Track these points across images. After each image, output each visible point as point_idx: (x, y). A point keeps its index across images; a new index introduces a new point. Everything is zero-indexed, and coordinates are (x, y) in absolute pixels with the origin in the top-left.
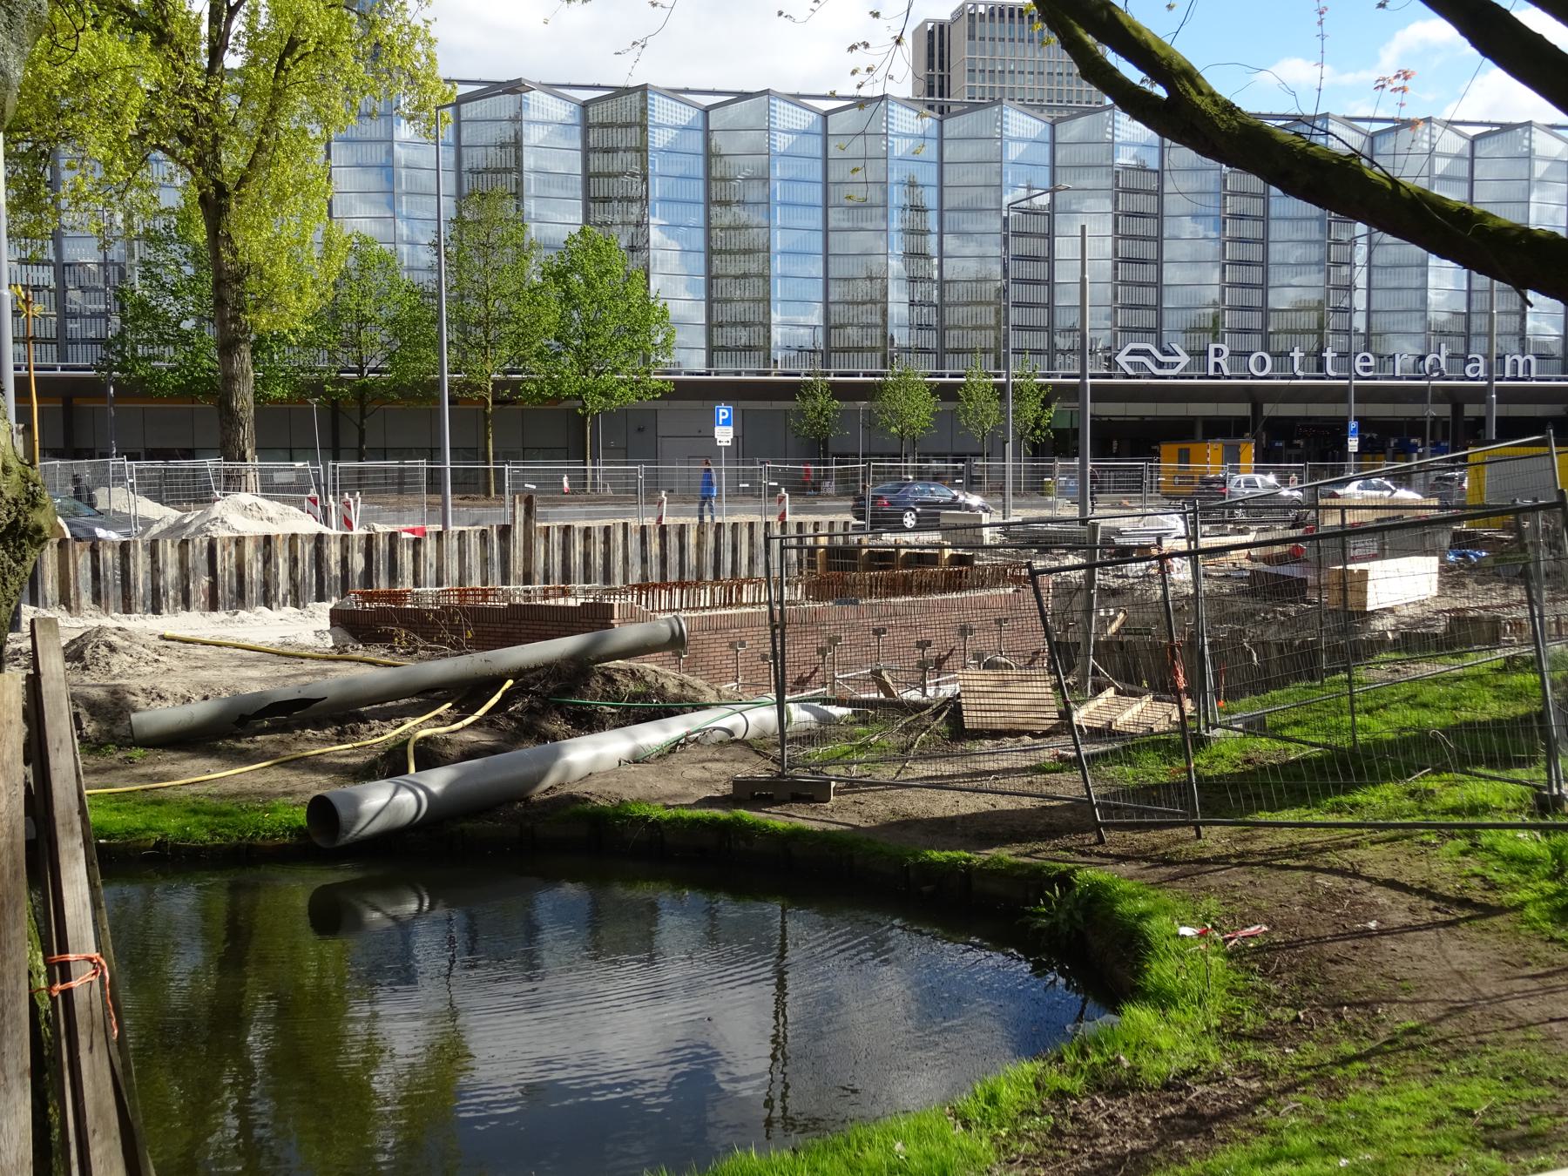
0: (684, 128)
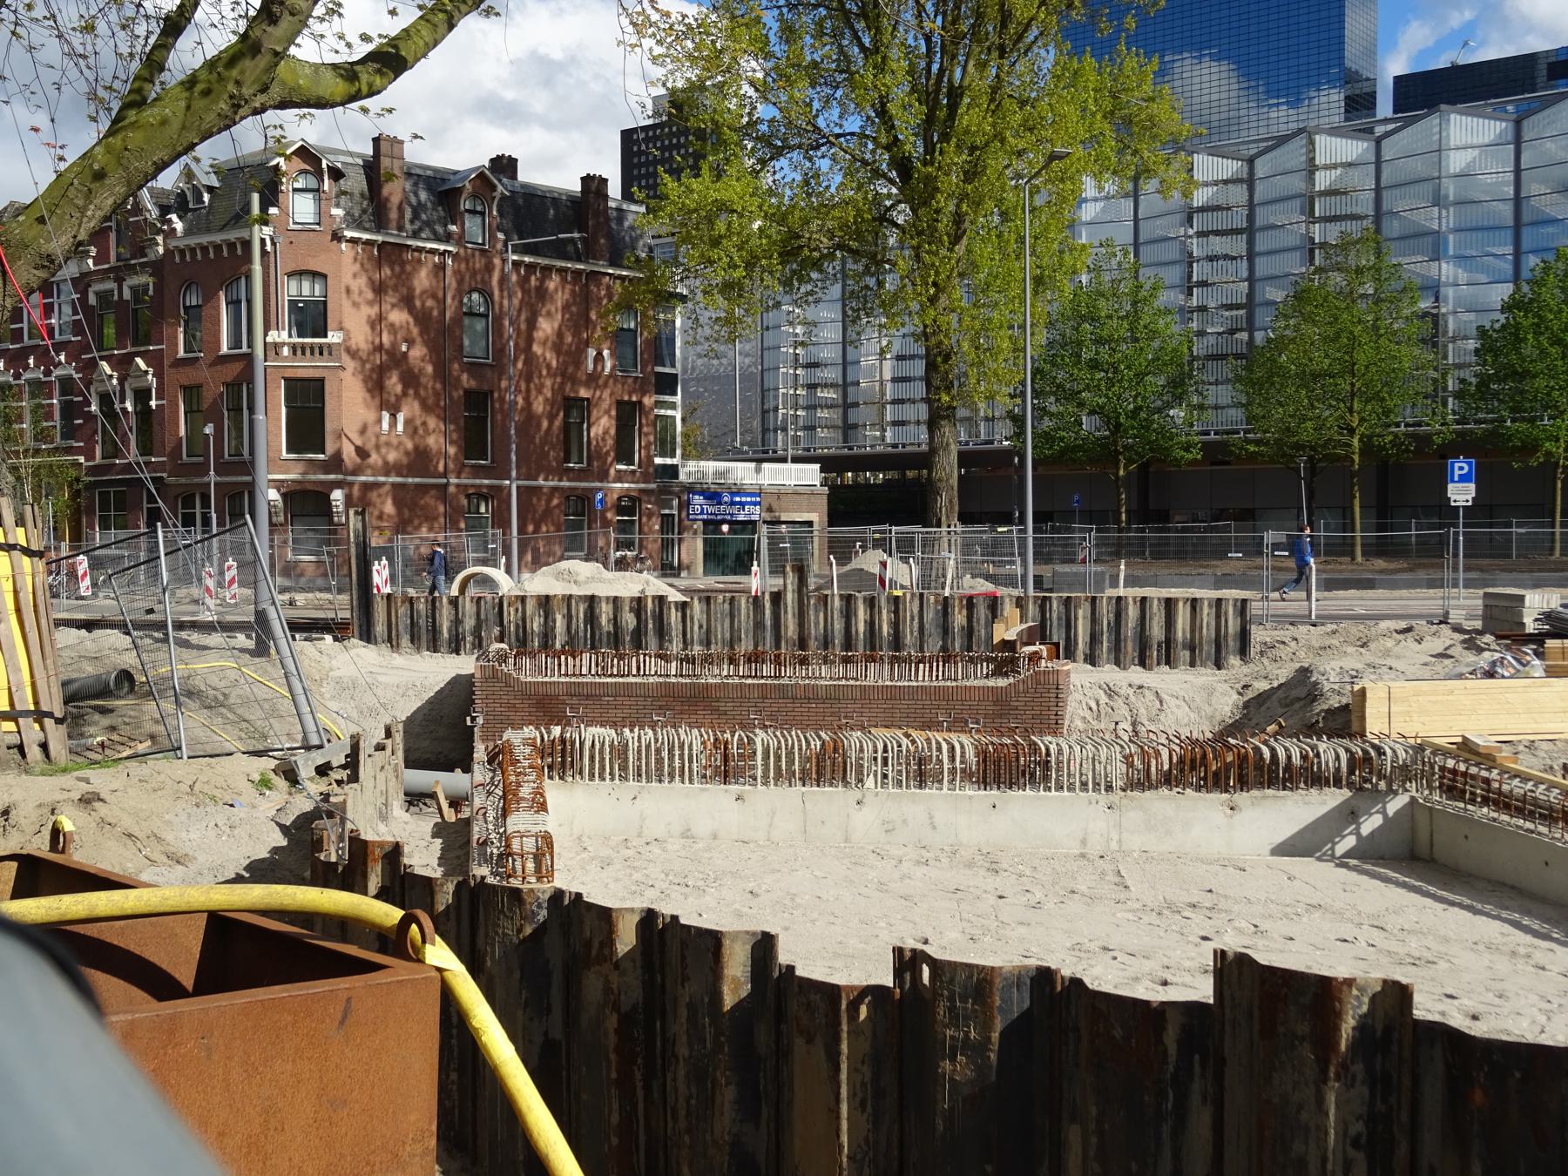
0: (1226, 182)
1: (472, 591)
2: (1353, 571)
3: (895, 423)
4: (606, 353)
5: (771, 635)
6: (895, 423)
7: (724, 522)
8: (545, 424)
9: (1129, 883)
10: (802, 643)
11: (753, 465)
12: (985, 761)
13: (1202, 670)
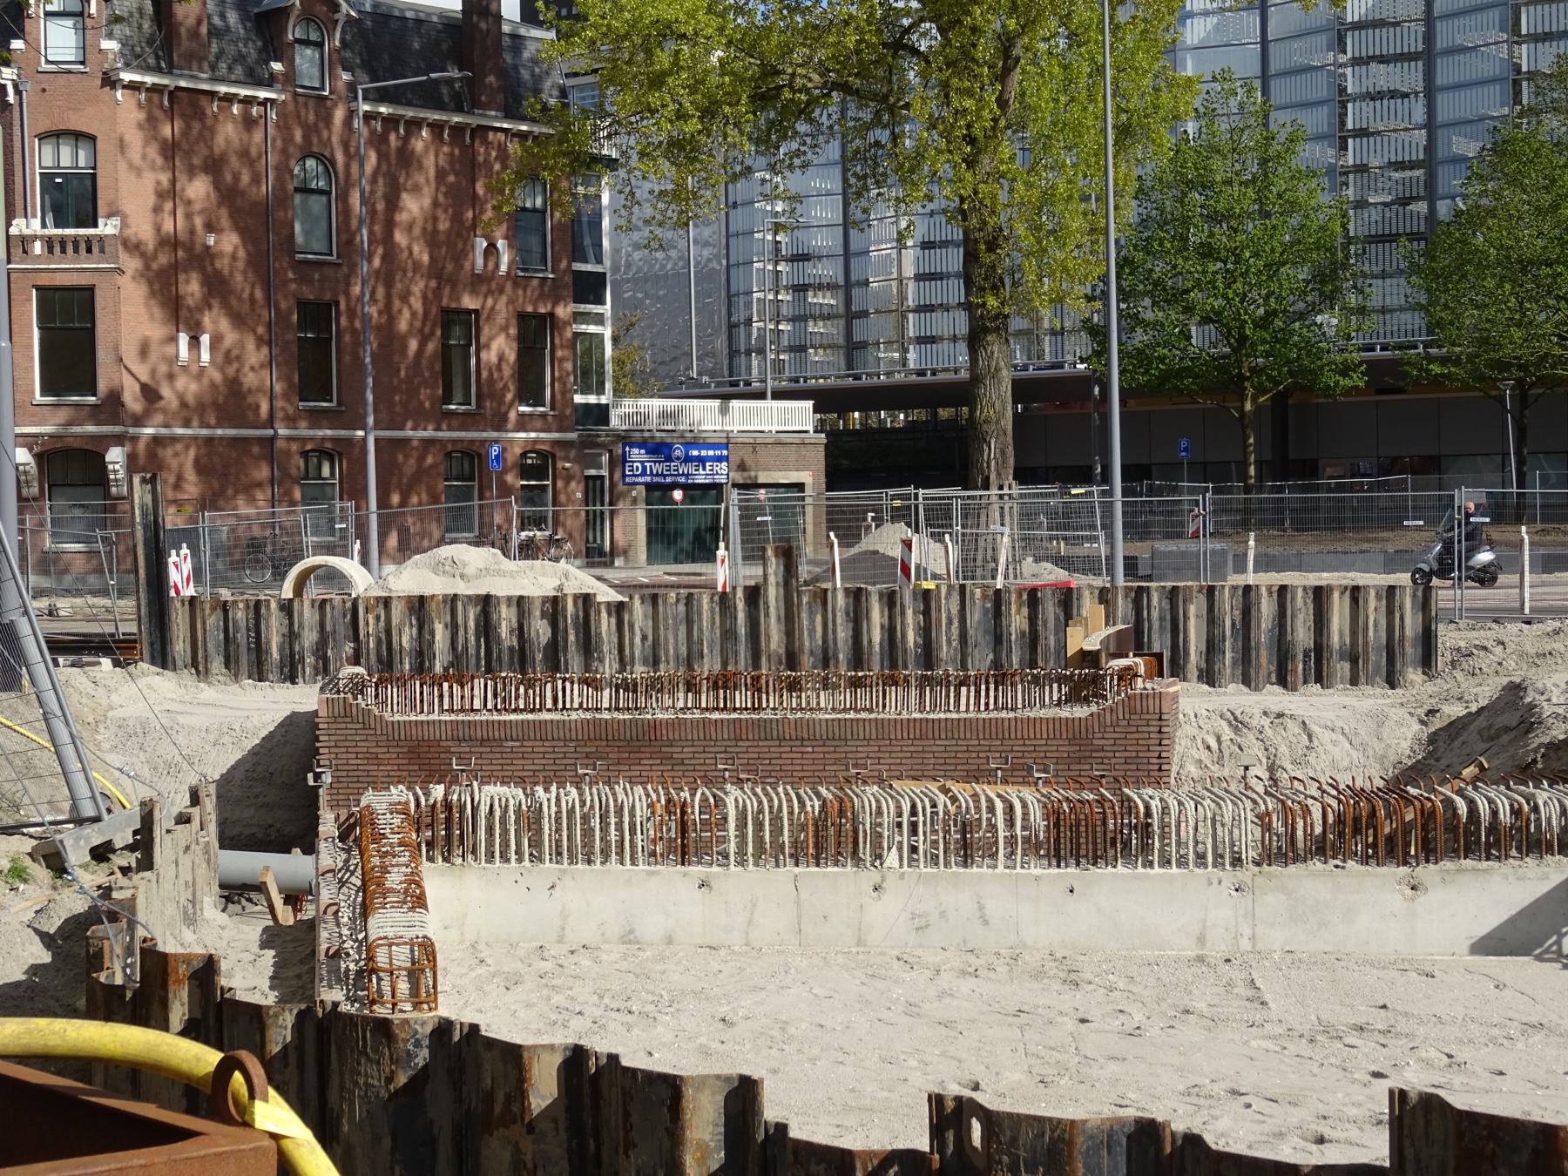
1: (313, 591)
4: (501, 244)
5: (748, 650)
8: (413, 345)
9: (1267, 997)
10: (792, 660)
11: (716, 403)
12: (1057, 825)
13: (1369, 690)
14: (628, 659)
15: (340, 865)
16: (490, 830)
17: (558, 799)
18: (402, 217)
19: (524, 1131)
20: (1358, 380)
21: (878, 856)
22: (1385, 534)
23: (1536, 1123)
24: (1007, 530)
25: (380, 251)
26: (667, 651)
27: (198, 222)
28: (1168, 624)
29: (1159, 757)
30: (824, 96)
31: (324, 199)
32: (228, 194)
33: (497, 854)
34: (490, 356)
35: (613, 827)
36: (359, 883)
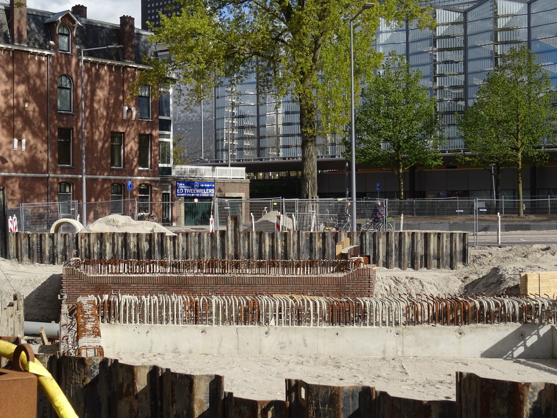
0: (453, 24)
1: (62, 232)
2: (519, 221)
3: (284, 147)
4: (133, 109)
5: (219, 257)
6: (284, 147)
7: (195, 197)
8: (100, 144)
9: (408, 371)
10: (237, 256)
11: (211, 168)
12: (332, 311)
13: (444, 270)
14: (177, 257)
15: (69, 323)
16: (125, 311)
17: (150, 301)
18: (97, 98)
19: (134, 398)
20: (440, 162)
21: (267, 321)
22: (449, 217)
23: (510, 382)
24: (315, 212)
25: (88, 111)
26: (191, 254)
27: (21, 100)
28: (372, 246)
29: (369, 292)
30: (250, 57)
31: (68, 91)
32: (33, 91)
33: (127, 320)
34: (128, 149)
35: (170, 310)
36: (76, 330)
